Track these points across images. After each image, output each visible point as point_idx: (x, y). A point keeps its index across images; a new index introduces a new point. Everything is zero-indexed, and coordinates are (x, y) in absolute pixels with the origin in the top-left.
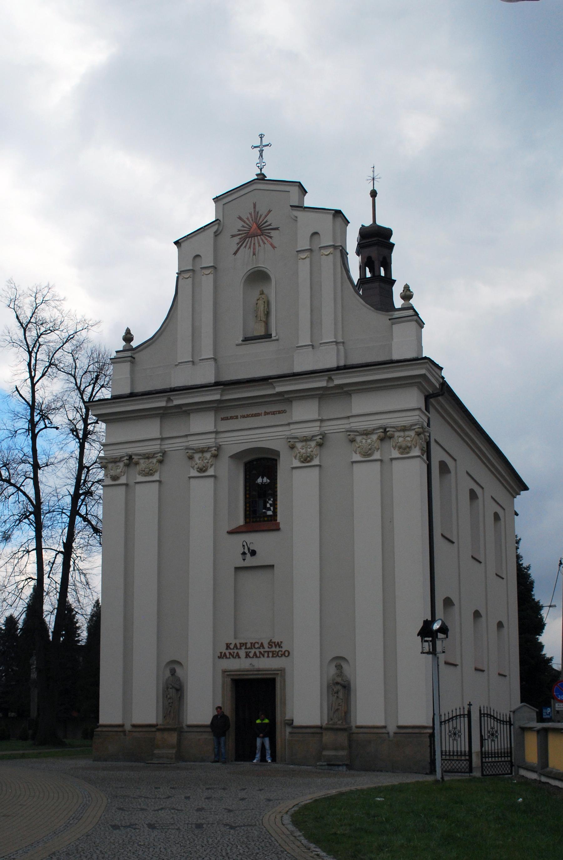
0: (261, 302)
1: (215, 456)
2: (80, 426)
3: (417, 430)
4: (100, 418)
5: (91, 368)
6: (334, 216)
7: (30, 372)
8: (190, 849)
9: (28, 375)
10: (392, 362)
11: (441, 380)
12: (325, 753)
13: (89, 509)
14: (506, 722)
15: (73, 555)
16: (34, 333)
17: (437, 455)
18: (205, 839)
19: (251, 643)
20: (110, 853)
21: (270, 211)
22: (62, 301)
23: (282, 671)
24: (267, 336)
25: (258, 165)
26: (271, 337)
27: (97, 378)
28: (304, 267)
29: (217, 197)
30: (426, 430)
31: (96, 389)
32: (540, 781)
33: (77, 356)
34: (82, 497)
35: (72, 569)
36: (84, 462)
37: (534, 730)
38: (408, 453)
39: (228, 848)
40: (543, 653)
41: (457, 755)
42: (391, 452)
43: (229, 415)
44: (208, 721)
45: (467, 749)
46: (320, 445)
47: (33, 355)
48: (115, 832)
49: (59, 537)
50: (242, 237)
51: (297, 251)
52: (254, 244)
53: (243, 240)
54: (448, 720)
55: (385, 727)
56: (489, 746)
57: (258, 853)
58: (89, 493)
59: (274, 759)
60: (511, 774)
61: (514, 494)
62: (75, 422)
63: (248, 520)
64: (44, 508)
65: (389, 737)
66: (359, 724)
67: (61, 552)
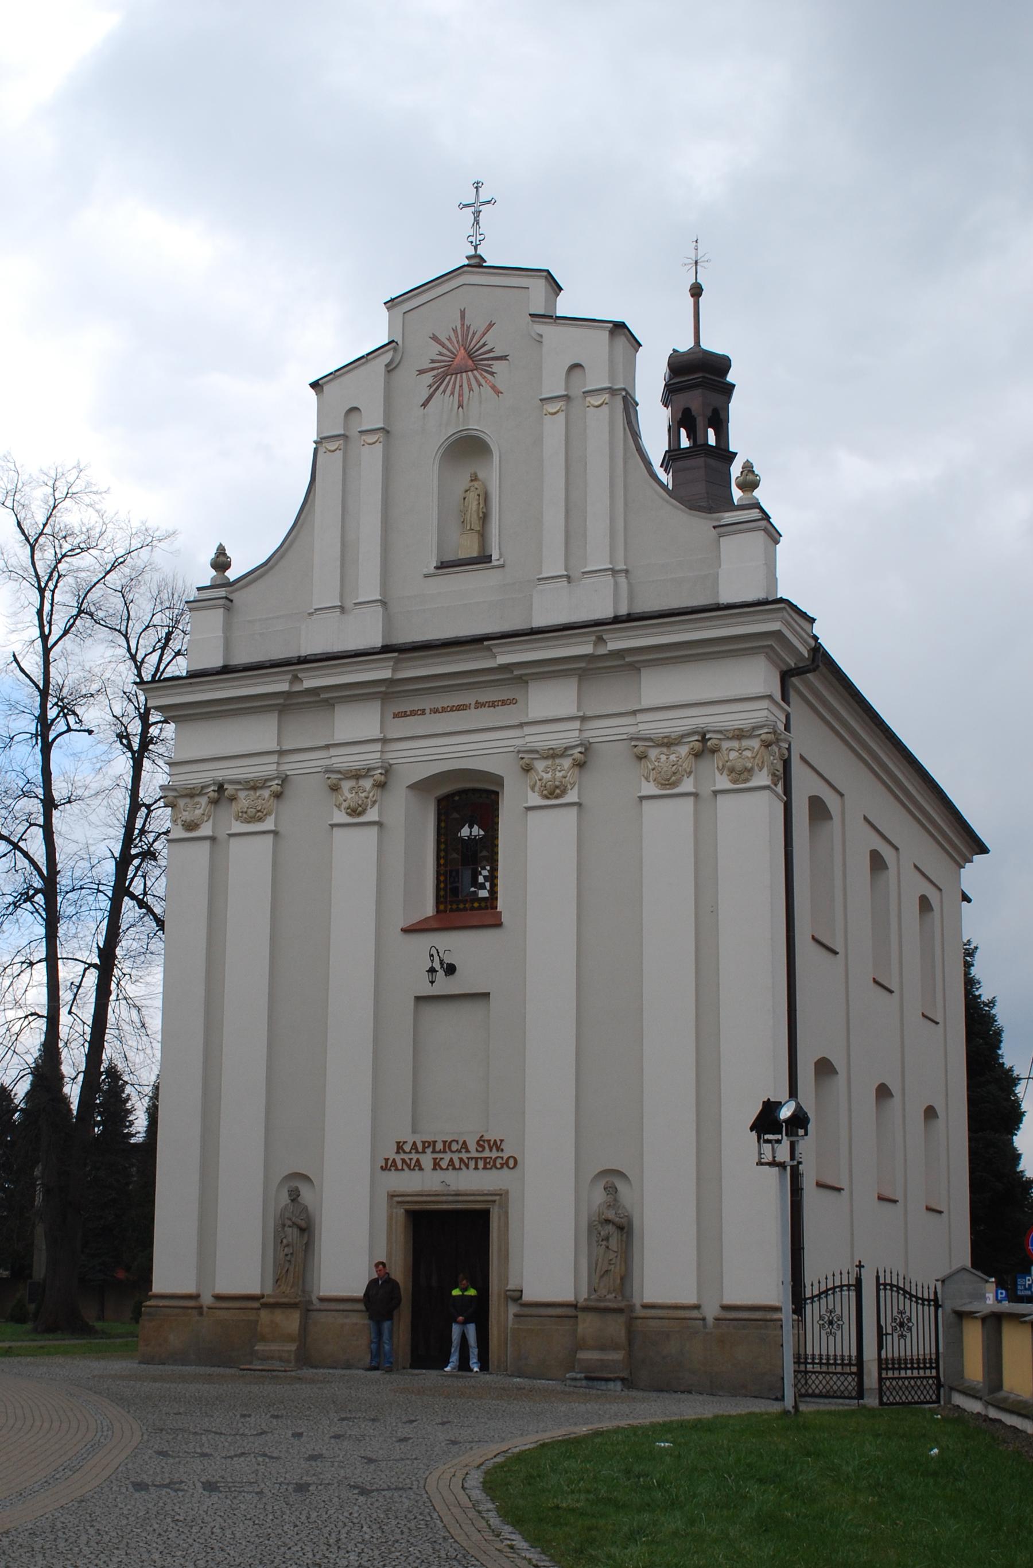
0: (472, 496)
1: (381, 786)
2: (135, 727)
3: (763, 737)
4: (173, 714)
5: (156, 620)
6: (612, 332)
7: (41, 626)
8: (270, 1530)
9: (37, 632)
10: (718, 607)
11: (813, 643)
12: (582, 1355)
13: (149, 884)
14: (929, 1300)
15: (116, 971)
16: (49, 554)
17: (805, 784)
18: (304, 1513)
19: (445, 1142)
20: (114, 1534)
21: (491, 325)
22: (104, 495)
23: (502, 1196)
24: (484, 559)
25: (470, 239)
26: (490, 562)
27: (168, 637)
28: (554, 429)
29: (392, 300)
30: (782, 737)
31: (167, 658)
32: (986, 1419)
33: (131, 597)
34: (136, 862)
35: (113, 997)
36: (141, 795)
37: (976, 1318)
38: (746, 780)
39: (344, 1531)
40: (1020, 1168)
41: (828, 1364)
42: (641, 782)
43: (408, 709)
44: (358, 1290)
45: (854, 1353)
46: (580, 765)
47: (48, 594)
48: (137, 1495)
49: (90, 938)
50: (438, 374)
51: (541, 400)
52: (461, 386)
53: (440, 379)
54: (819, 1296)
55: (697, 1307)
56: (894, 1348)
57: (397, 1541)
58: (149, 855)
59: (484, 1367)
60: (938, 1401)
61: (961, 861)
62: (125, 720)
63: (442, 907)
64: (64, 881)
65: (705, 1326)
66: (648, 1299)
67: (95, 966)
